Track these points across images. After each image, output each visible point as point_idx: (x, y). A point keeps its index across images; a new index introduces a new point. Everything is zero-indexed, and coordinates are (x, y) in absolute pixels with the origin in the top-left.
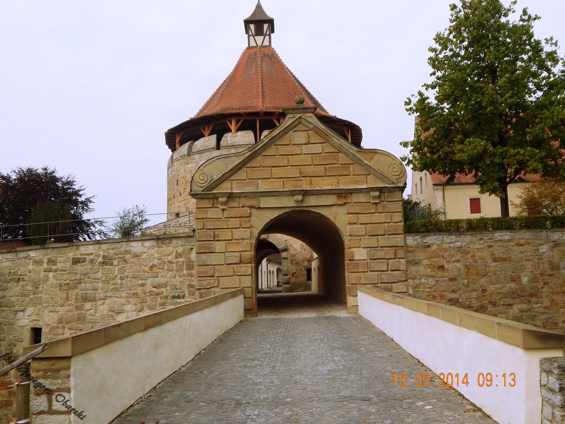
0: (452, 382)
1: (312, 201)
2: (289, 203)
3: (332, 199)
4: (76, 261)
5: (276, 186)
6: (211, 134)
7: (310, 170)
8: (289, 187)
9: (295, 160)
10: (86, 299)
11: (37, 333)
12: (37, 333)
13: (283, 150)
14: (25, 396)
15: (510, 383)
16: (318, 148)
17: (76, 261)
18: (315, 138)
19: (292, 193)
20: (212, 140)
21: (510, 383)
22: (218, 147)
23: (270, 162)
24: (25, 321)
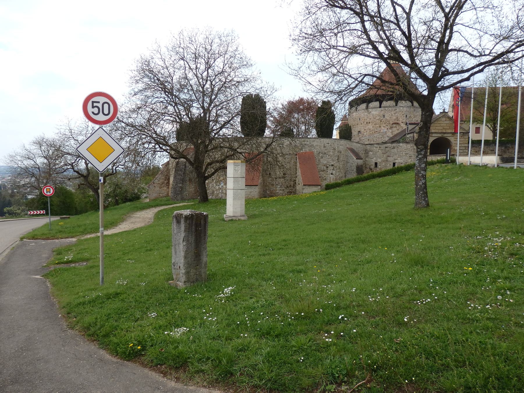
0: (136, 217)
1: (446, 135)
2: (440, 135)
3: (451, 135)
4: (386, 147)
5: (437, 131)
6: (376, 101)
7: (446, 127)
8: (440, 131)
9: (442, 125)
10: (388, 156)
11: (376, 164)
12: (376, 164)
13: (439, 122)
14: (88, 178)
15: (93, 113)
16: (448, 122)
17: (386, 147)
18: (448, 120)
19: (440, 133)
20: (377, 104)
21: (93, 113)
22: (380, 107)
23: (436, 125)
24: (374, 160)
